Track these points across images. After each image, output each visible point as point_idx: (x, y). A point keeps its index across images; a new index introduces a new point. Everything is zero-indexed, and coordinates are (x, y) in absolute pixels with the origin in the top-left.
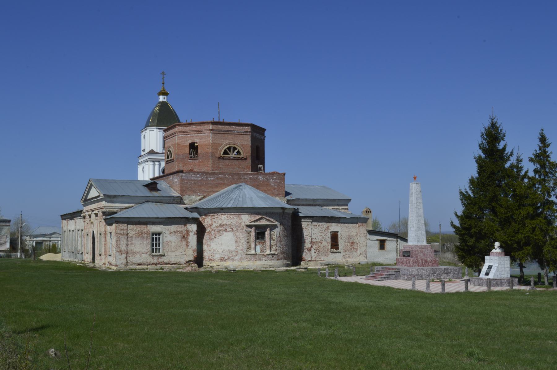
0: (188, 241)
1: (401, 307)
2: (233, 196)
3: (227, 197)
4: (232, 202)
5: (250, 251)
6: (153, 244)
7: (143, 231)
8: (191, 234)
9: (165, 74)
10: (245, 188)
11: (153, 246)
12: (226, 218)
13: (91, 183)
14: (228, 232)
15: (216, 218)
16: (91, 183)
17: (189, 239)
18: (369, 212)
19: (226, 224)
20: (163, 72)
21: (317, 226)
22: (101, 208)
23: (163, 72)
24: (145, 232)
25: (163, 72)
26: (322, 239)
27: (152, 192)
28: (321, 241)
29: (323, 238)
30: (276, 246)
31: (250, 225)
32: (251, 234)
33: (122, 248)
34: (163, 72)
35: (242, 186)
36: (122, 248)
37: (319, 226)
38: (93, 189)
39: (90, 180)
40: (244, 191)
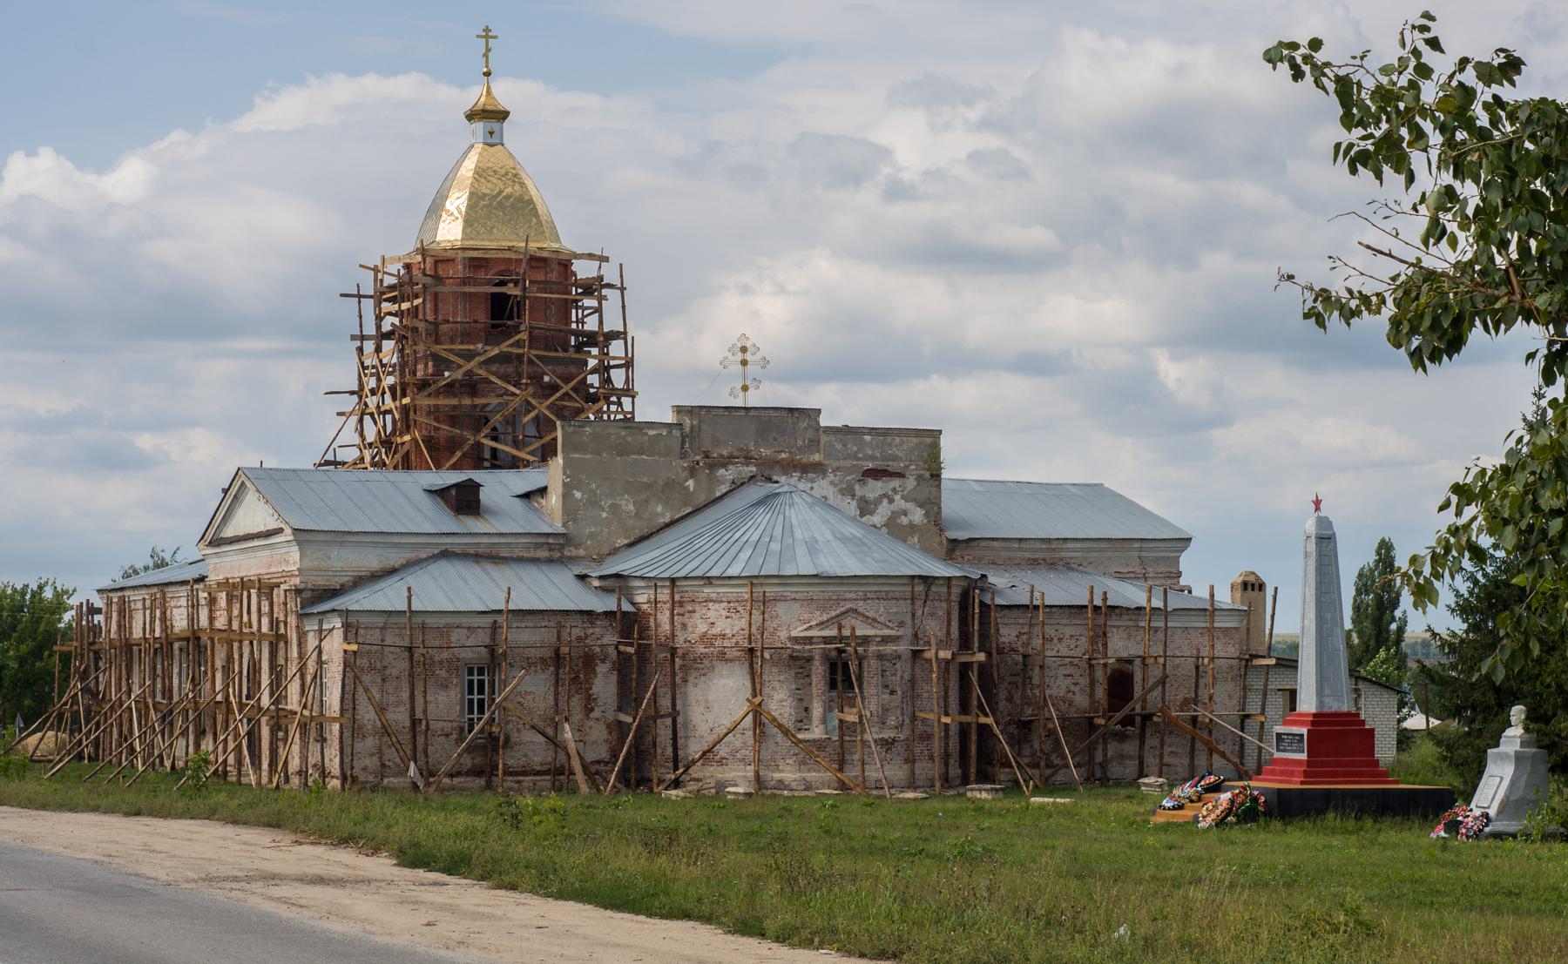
0: (591, 692)
1: (1345, 932)
2: (749, 533)
3: (726, 538)
4: (744, 555)
5: (806, 730)
6: (471, 702)
7: (437, 658)
8: (602, 668)
9: (496, 37)
10: (791, 505)
11: (471, 692)
12: (724, 613)
13: (243, 483)
14: (731, 661)
15: (689, 612)
16: (243, 483)
17: (594, 687)
18: (1257, 587)
19: (724, 635)
20: (484, 30)
21: (1055, 641)
22: (284, 574)
23: (484, 30)
24: (441, 662)
25: (487, 30)
26: (1072, 688)
27: (461, 517)
28: (1070, 694)
29: (1075, 684)
30: (899, 712)
31: (806, 637)
32: (810, 669)
33: (367, 716)
34: (487, 30)
35: (781, 499)
36: (367, 716)
37: (1060, 640)
38: (251, 497)
39: (240, 472)
40: (787, 514)
